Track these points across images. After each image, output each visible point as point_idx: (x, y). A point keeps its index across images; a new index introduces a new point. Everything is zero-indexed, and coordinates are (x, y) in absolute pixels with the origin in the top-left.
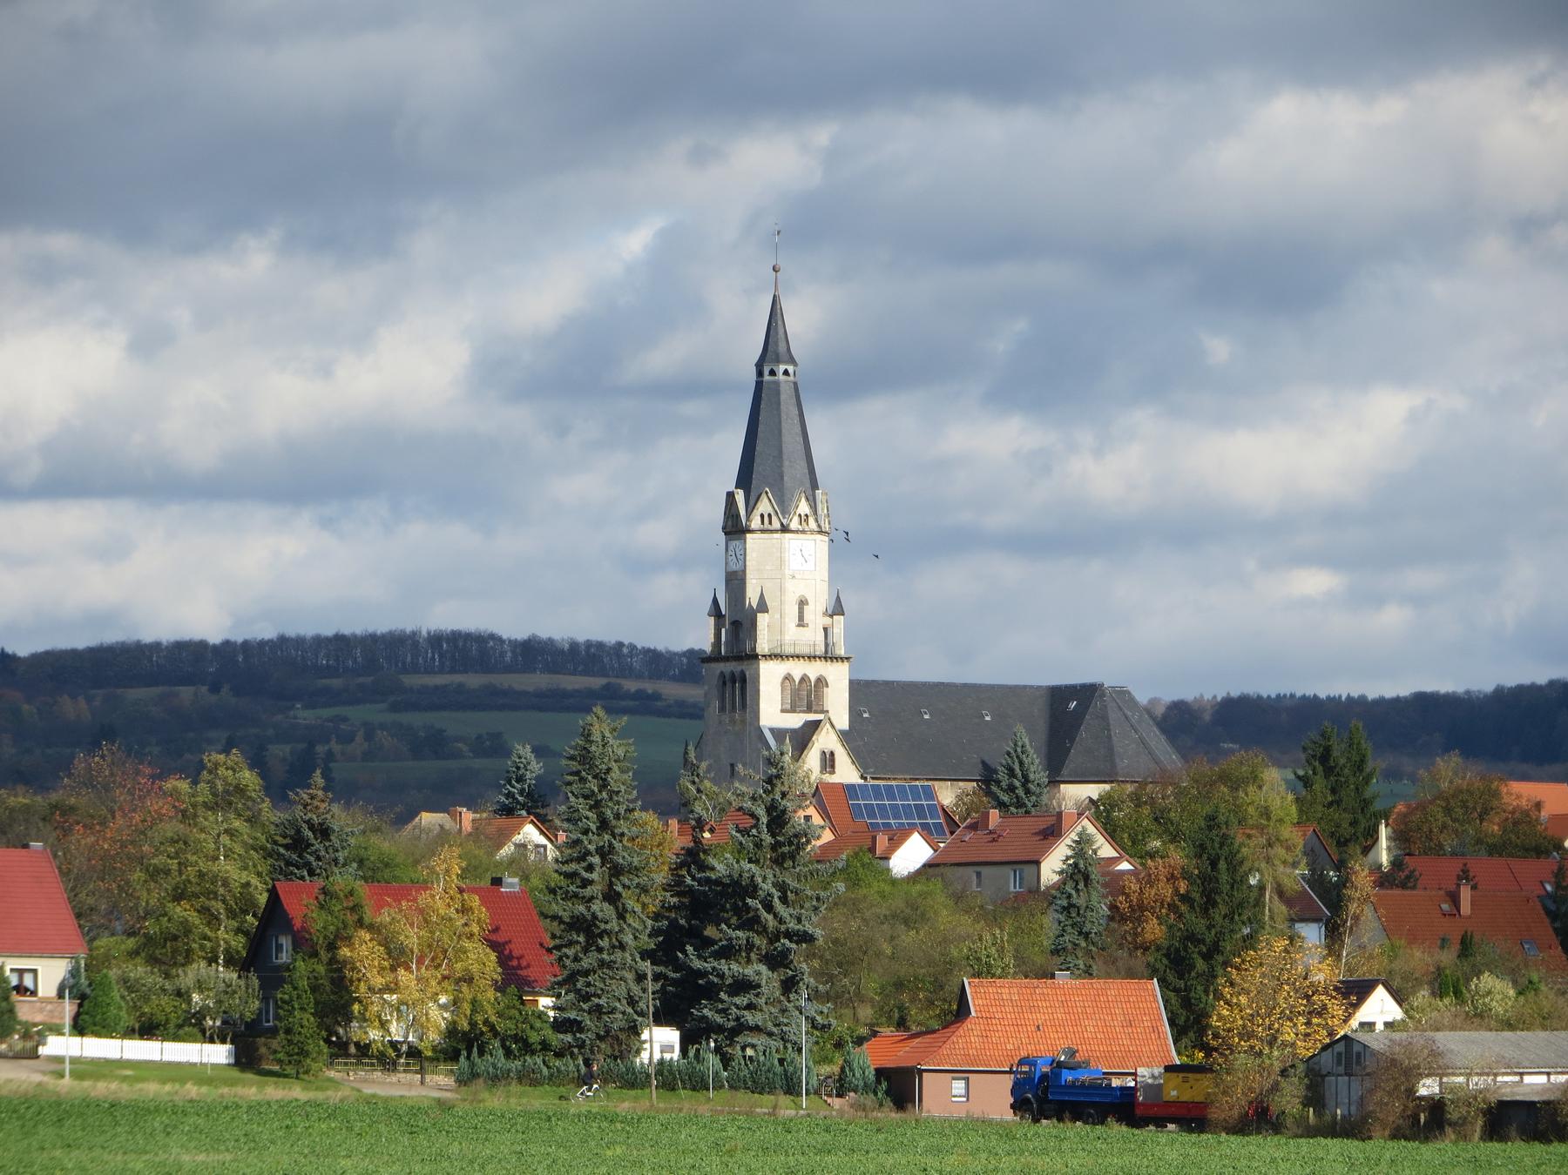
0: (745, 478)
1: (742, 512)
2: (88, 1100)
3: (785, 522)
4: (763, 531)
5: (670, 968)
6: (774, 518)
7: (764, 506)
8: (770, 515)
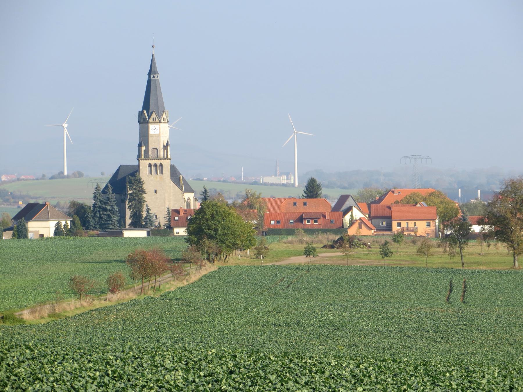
4: (164, 123)
7: (154, 116)
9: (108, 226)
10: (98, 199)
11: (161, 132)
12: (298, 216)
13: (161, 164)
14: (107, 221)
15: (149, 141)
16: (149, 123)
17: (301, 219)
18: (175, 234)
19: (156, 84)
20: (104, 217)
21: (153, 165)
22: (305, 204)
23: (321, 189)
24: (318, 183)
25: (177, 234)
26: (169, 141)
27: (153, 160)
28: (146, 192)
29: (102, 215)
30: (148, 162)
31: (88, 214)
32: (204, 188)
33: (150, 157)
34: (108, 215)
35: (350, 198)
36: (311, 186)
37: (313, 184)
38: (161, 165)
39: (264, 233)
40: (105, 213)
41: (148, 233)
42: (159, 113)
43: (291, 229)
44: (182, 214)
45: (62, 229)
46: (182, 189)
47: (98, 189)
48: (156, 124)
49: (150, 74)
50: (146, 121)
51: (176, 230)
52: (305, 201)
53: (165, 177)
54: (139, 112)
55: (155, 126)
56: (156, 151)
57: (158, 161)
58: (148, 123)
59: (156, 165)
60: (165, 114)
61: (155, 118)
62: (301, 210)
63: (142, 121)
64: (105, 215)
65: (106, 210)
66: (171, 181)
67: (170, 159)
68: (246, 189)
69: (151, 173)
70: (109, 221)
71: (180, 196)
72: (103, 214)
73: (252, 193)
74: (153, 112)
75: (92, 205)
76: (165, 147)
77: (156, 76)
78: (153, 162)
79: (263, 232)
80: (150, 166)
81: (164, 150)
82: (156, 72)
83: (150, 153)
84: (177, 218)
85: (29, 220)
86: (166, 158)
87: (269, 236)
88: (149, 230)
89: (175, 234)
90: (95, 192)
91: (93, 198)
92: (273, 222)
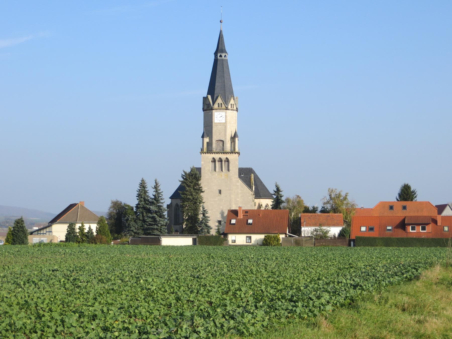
0: (211, 90)
1: (211, 103)
2: (140, 186)
3: (227, 106)
4: (232, 110)
5: (168, 210)
6: (223, 105)
7: (219, 101)
8: (233, 104)
9: (153, 232)
10: (142, 197)
11: (228, 121)
12: (398, 221)
13: (227, 158)
14: (152, 225)
15: (213, 131)
16: (214, 109)
17: (402, 225)
18: (230, 243)
19: (223, 65)
20: (148, 220)
21: (217, 159)
22: (404, 208)
23: (416, 197)
24: (412, 190)
25: (232, 242)
26: (236, 131)
27: (217, 153)
28: (203, 190)
29: (146, 218)
30: (211, 156)
31: (129, 217)
32: (276, 186)
33: (214, 150)
34: (153, 218)
35: (448, 207)
36: (405, 193)
37: (407, 190)
38: (227, 160)
39: (352, 243)
40: (150, 215)
41: (194, 241)
42: (225, 98)
43: (390, 238)
44: (241, 216)
45: (77, 233)
46: (252, 190)
47: (143, 186)
48: (222, 111)
49: (216, 54)
50: (210, 108)
51: (231, 237)
52: (405, 205)
53: (231, 175)
54: (204, 98)
55: (221, 113)
56: (221, 143)
57: (223, 155)
58: (212, 109)
59: (221, 160)
60: (234, 99)
61: (221, 104)
62: (399, 214)
63: (205, 108)
64: (150, 217)
65: (149, 211)
66: (239, 179)
67: (239, 153)
68: (329, 189)
69: (215, 170)
70: (154, 225)
71: (249, 198)
72: (148, 217)
73: (336, 193)
74: (218, 96)
75: (135, 206)
76: (233, 139)
77: (223, 55)
78: (217, 156)
79: (350, 241)
80: (214, 161)
81: (231, 143)
82: (224, 51)
83: (214, 145)
84: (233, 221)
85: (53, 223)
86: (233, 152)
87: (359, 248)
88: (195, 237)
89: (230, 243)
90: (139, 189)
91: (137, 196)
92: (363, 229)
